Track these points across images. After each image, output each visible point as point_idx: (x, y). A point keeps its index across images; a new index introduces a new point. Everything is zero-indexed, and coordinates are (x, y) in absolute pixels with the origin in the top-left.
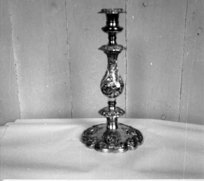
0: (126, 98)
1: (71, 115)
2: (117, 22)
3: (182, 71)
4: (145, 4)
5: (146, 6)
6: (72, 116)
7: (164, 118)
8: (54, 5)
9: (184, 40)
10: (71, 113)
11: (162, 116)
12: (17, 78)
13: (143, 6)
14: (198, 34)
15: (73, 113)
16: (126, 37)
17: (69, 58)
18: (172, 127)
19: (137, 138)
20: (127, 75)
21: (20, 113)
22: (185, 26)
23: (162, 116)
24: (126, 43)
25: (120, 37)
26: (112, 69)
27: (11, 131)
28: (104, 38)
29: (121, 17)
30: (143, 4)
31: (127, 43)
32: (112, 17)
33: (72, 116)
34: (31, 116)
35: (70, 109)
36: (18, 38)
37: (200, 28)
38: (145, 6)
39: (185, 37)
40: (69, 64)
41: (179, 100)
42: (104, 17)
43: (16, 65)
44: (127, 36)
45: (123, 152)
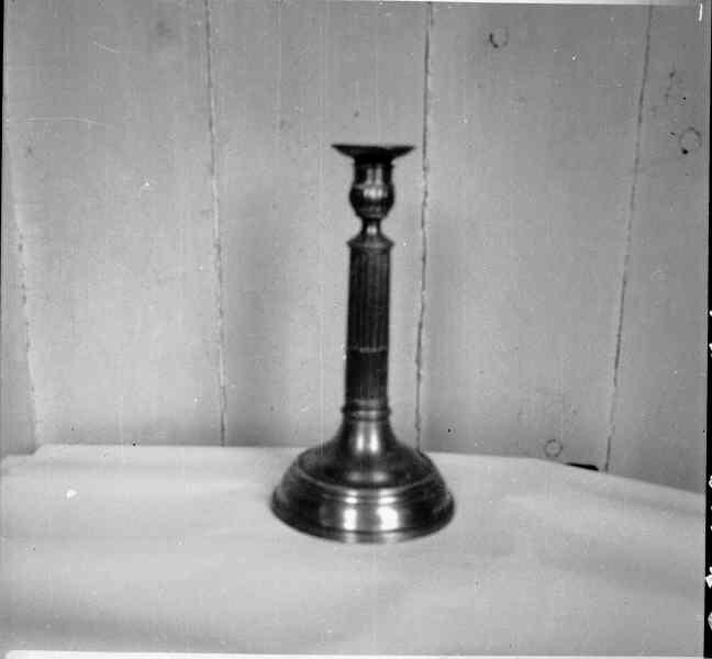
0: (419, 375)
1: (247, 434)
2: (378, 227)
3: (625, 283)
4: (496, 39)
5: (500, 44)
6: (223, 438)
7: (556, 451)
8: (163, 30)
9: (636, 171)
10: (220, 429)
11: (550, 442)
12: (24, 298)
13: (490, 47)
14: (685, 152)
15: (226, 427)
16: (425, 157)
17: (216, 227)
18: (656, 506)
19: (427, 509)
20: (424, 293)
21: (32, 423)
22: (640, 120)
23: (550, 442)
24: (425, 176)
25: (390, 226)
26: (346, 505)
27: (32, 487)
28: (354, 225)
29: (400, 166)
30: (491, 37)
31: (429, 176)
32: (373, 160)
33: (223, 438)
34: (72, 435)
35: (219, 415)
36: (30, 151)
37: (692, 129)
38: (496, 46)
39: (637, 161)
40: (215, 251)
41: (612, 389)
42: (346, 166)
43: (21, 247)
44: (428, 152)
45: (401, 541)
